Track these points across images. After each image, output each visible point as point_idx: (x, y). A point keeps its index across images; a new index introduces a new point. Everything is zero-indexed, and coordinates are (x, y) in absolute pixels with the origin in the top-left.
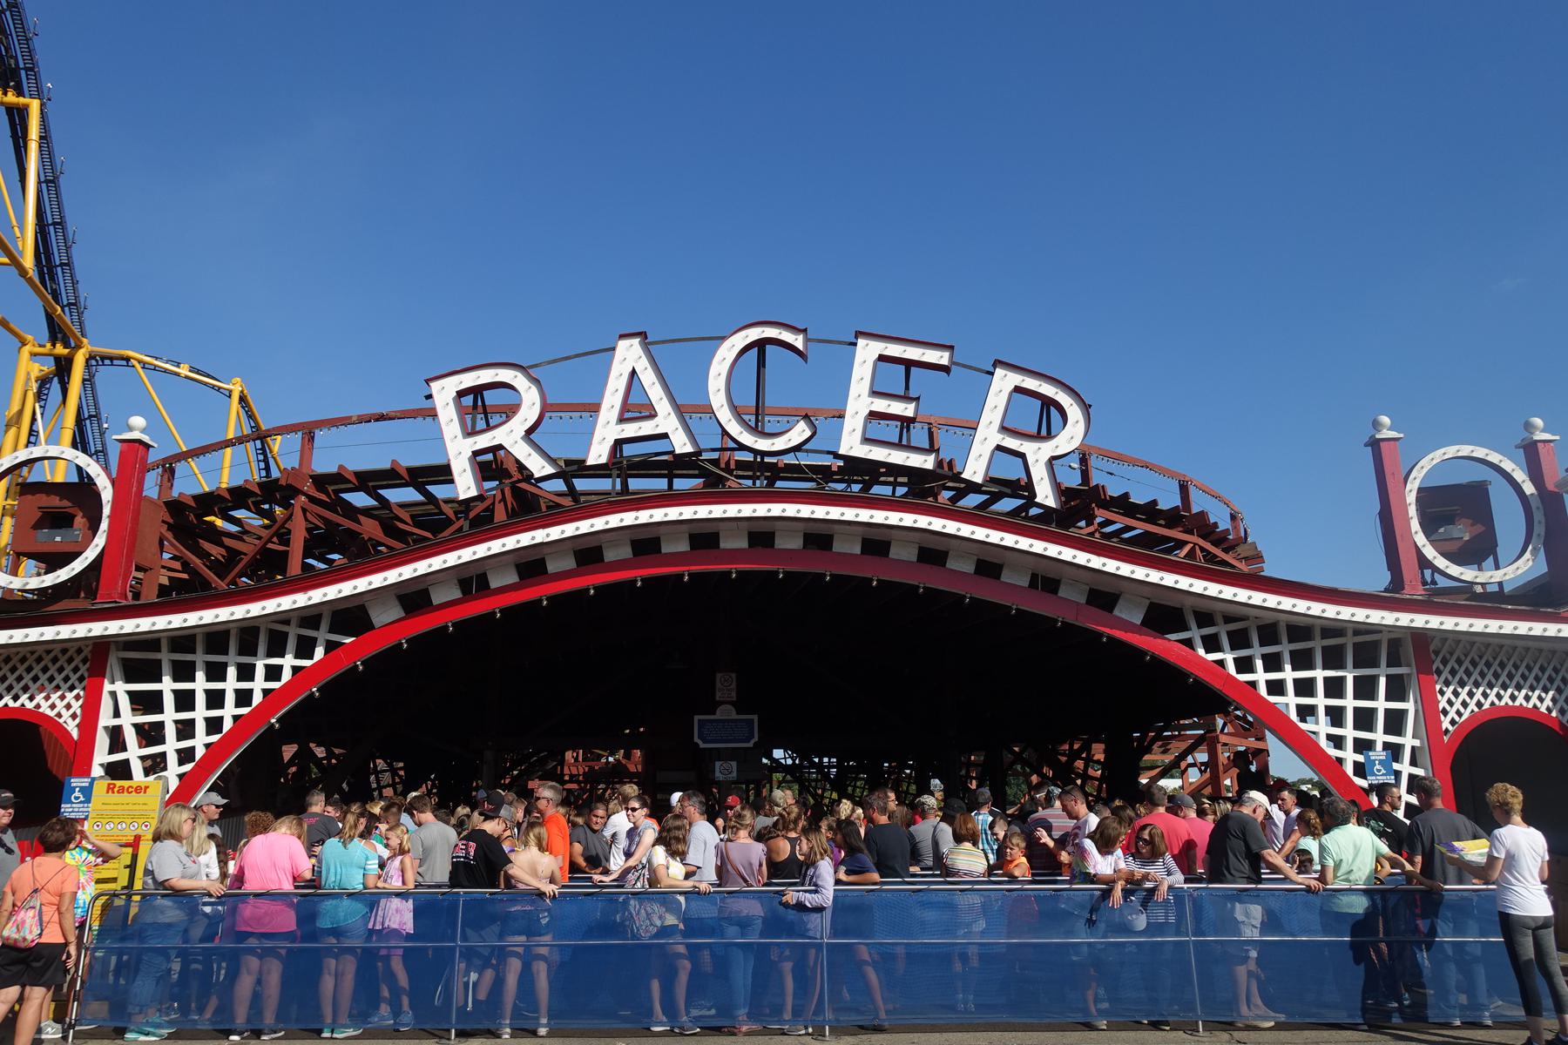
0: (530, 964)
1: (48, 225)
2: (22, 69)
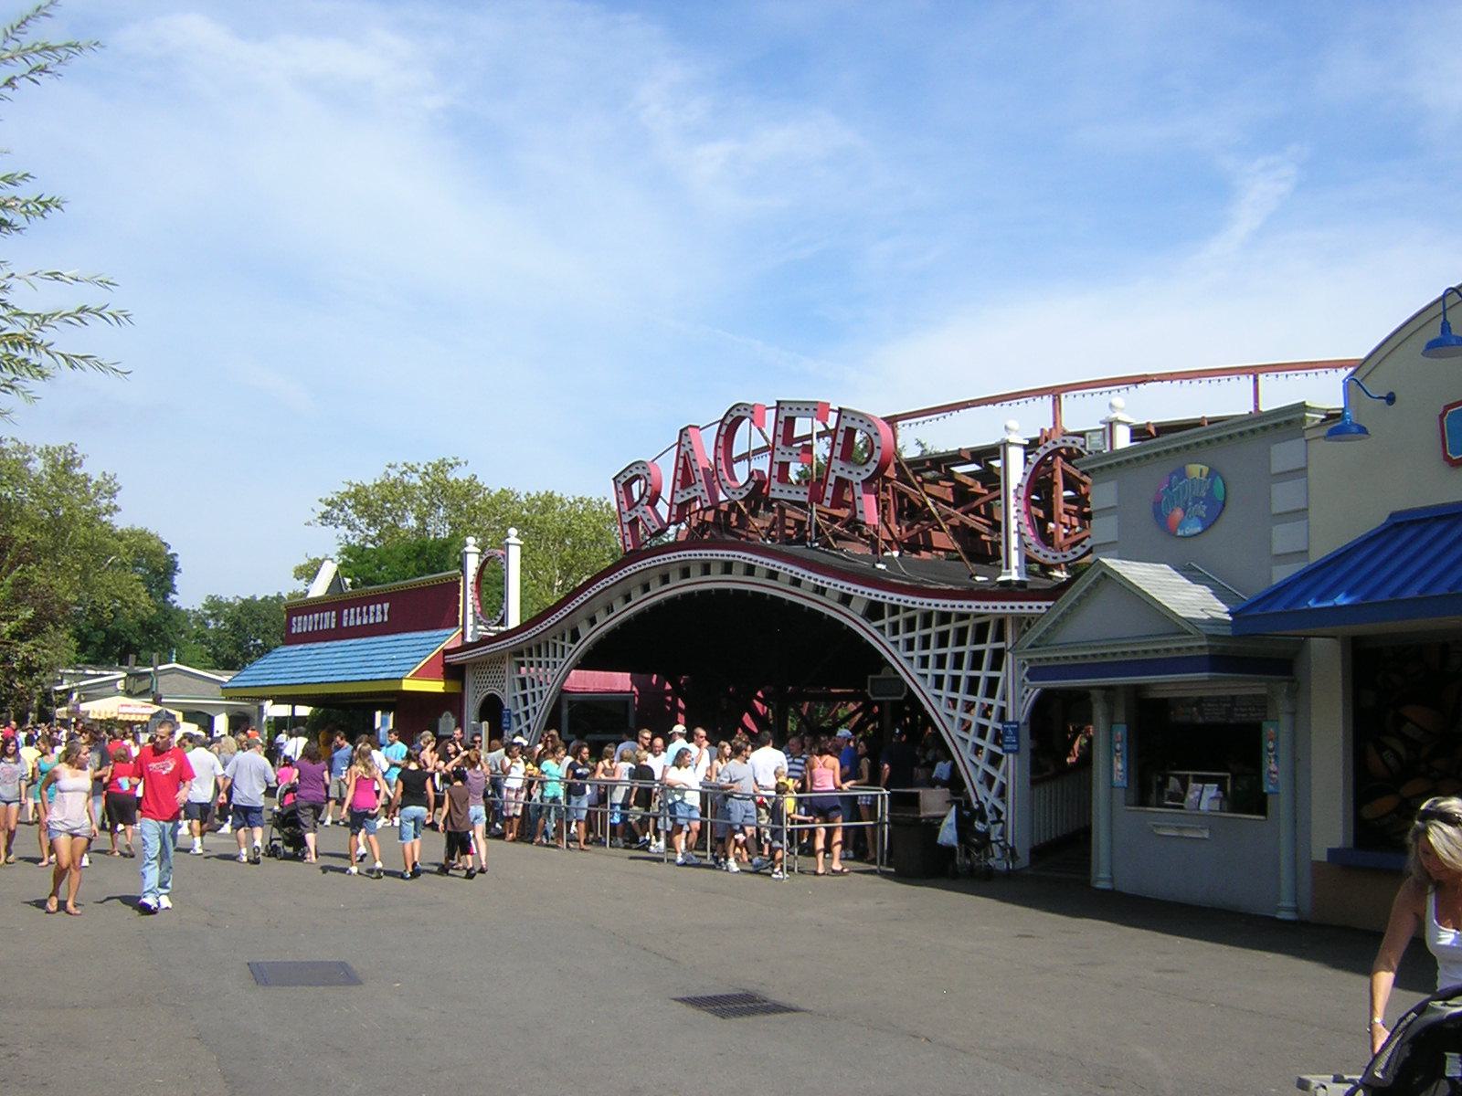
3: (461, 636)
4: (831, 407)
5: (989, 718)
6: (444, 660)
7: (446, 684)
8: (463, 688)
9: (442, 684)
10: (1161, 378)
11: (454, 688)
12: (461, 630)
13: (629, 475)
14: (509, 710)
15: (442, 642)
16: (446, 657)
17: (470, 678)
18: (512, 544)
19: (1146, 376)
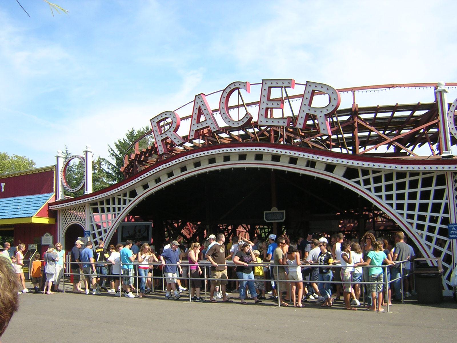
3: (54, 197)
4: (296, 82)
5: (437, 217)
6: (48, 208)
7: (49, 220)
8: (56, 221)
9: (47, 220)
10: (400, 86)
11: (53, 222)
12: (55, 194)
13: (160, 118)
14: (89, 231)
15: (48, 199)
16: (49, 207)
17: (60, 217)
18: (89, 152)
19: (393, 85)
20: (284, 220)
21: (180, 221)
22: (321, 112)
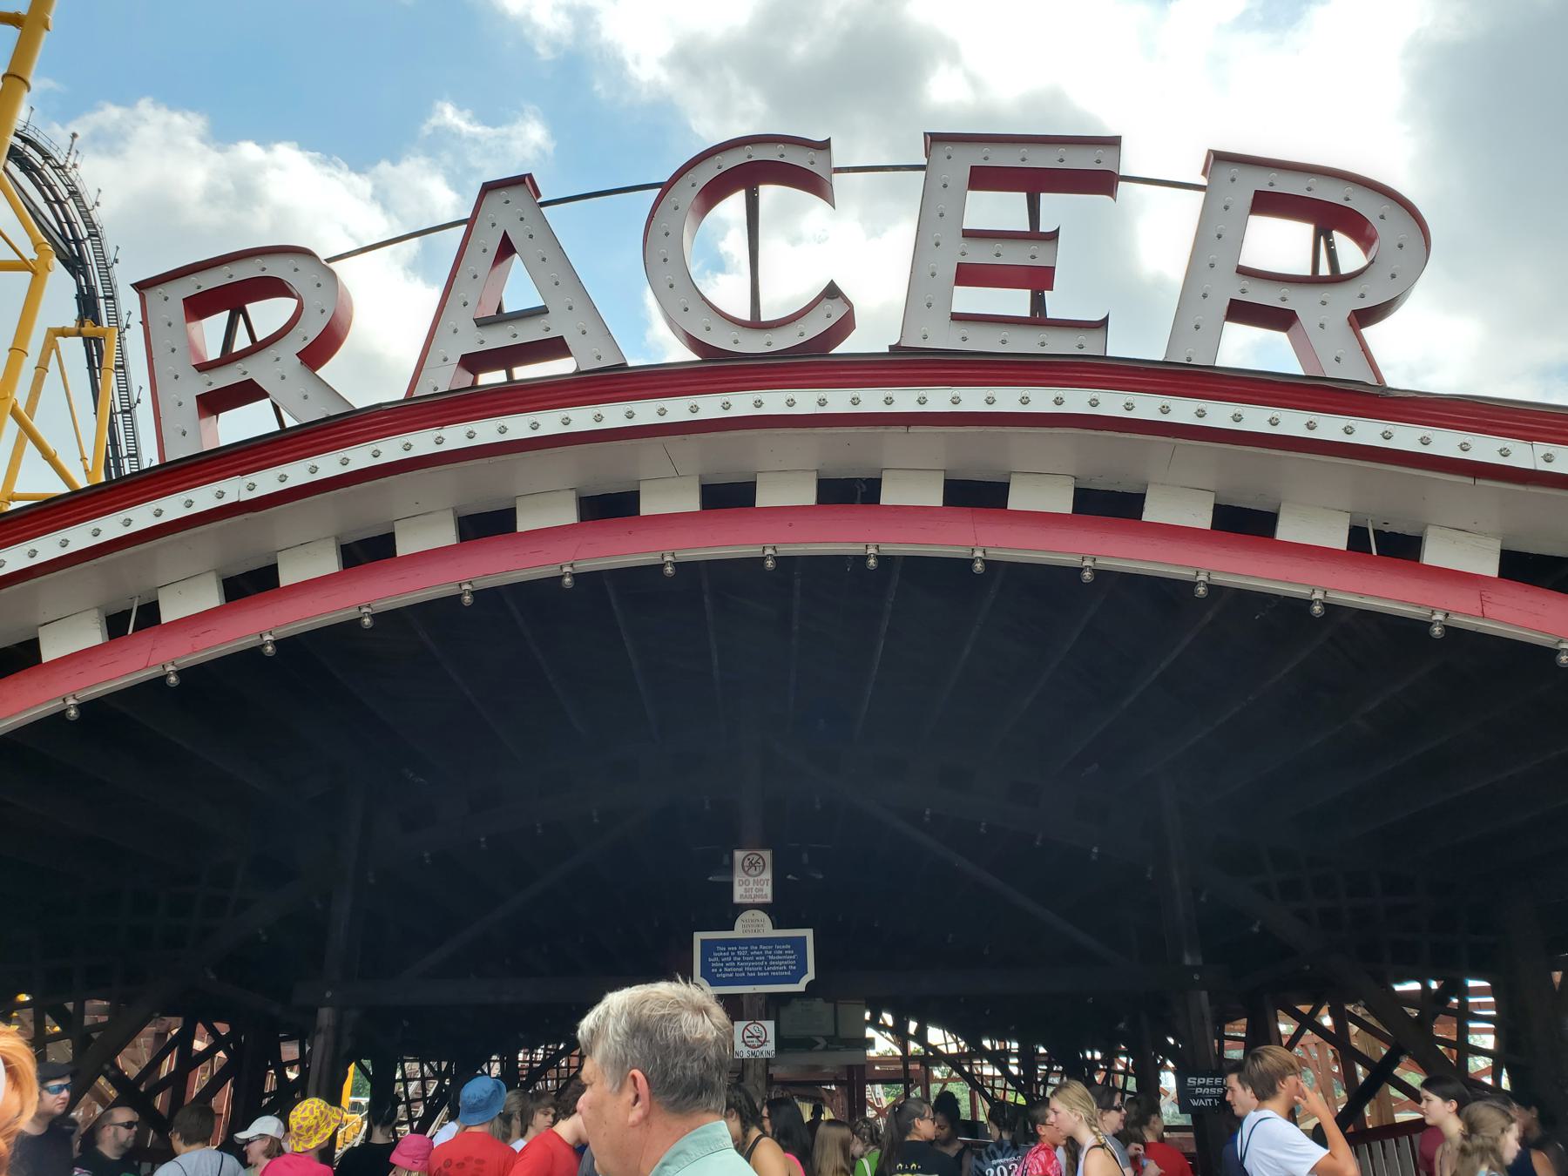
0: (317, 1011)
1: (123, 458)
2: (101, 298)
20: (809, 985)
21: (1434, 985)
22: (1324, 303)
